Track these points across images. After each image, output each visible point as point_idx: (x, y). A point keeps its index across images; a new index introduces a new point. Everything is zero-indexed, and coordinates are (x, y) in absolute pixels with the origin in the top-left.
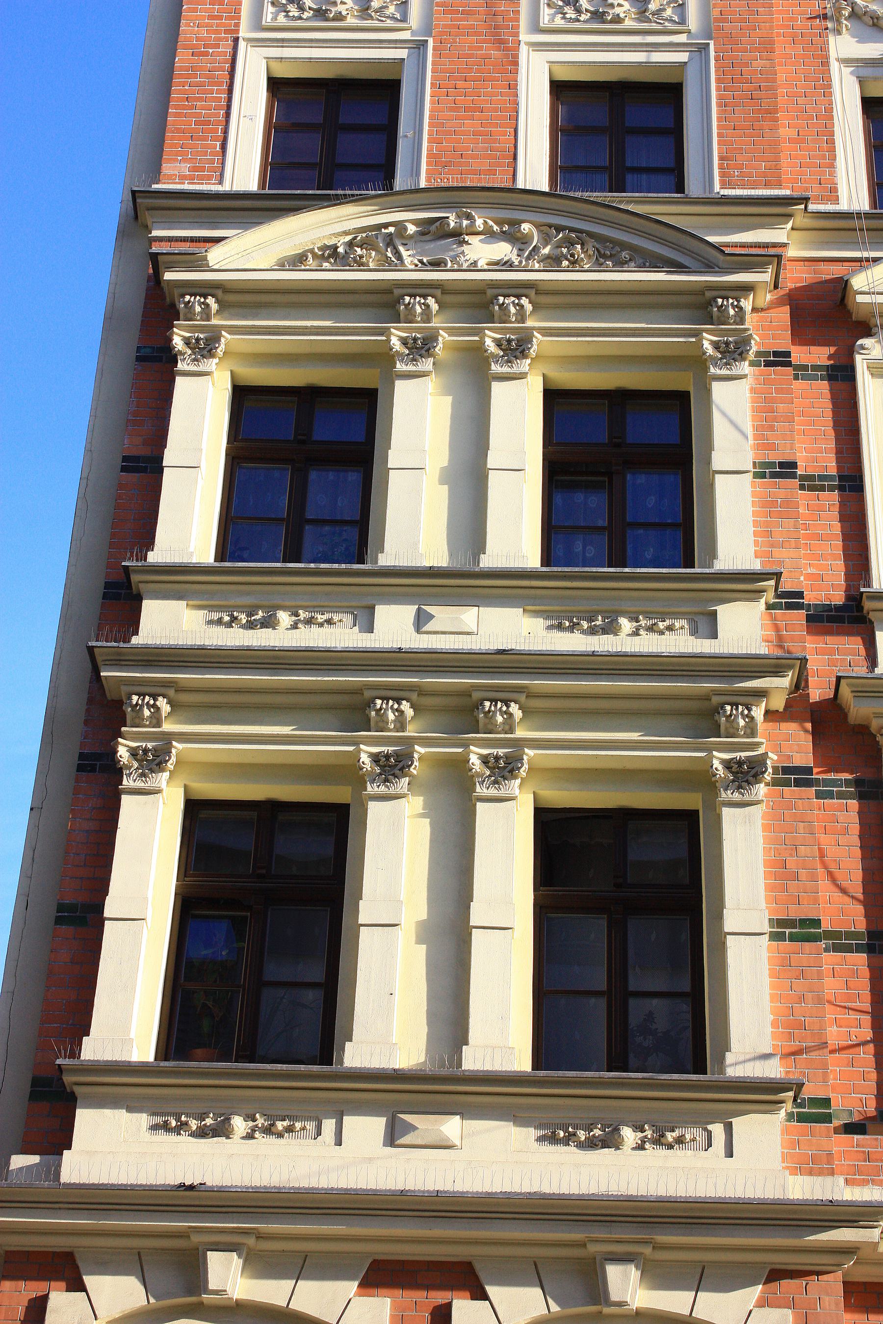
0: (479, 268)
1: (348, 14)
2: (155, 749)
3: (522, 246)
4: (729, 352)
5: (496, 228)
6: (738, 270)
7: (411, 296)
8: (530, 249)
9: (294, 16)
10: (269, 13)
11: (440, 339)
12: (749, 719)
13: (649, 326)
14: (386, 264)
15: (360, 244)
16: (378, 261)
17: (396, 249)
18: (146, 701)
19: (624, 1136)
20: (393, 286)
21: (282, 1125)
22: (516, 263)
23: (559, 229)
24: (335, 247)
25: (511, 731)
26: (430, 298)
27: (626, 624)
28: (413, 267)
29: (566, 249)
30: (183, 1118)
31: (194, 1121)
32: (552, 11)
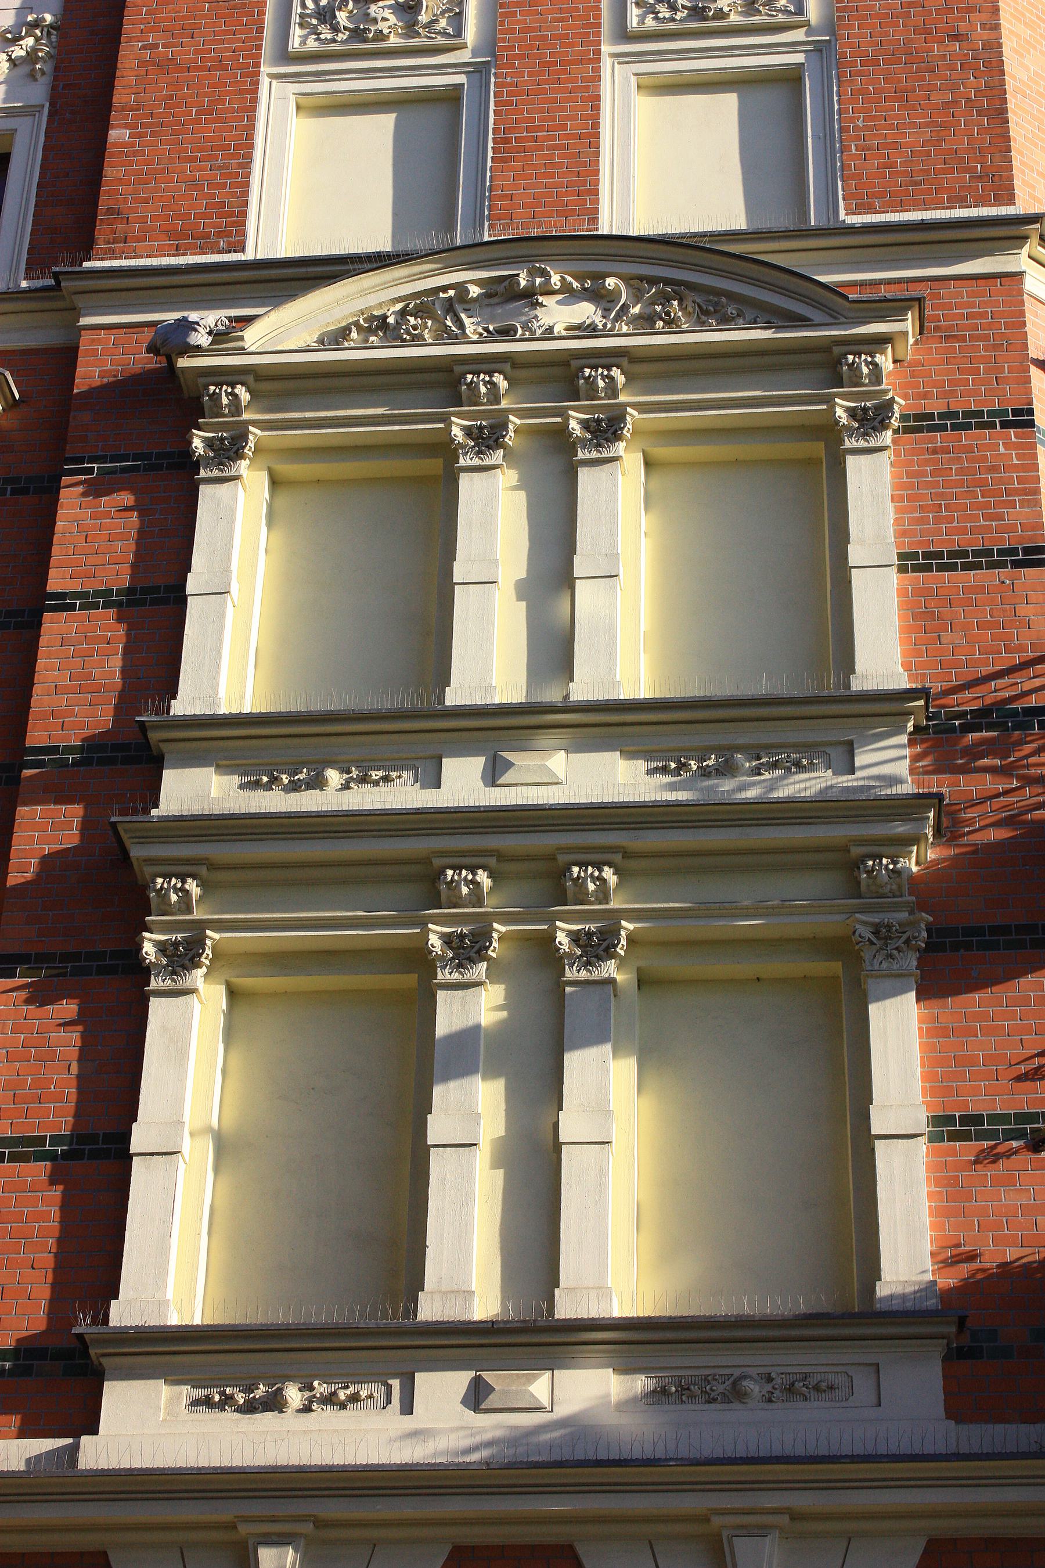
0: (556, 335)
1: (731, 10)
2: (472, 933)
3: (609, 305)
4: (867, 420)
5: (575, 284)
6: (871, 320)
7: (591, 368)
8: (618, 308)
9: (664, 18)
10: (634, 17)
11: (628, 418)
12: (183, 893)
13: (766, 393)
14: (445, 336)
15: (414, 312)
16: (436, 331)
17: (457, 316)
18: (463, 876)
19: (288, 1396)
20: (452, 363)
21: (344, 1394)
22: (601, 327)
23: (652, 281)
24: (385, 317)
25: (606, 900)
26: (614, 369)
27: (334, 777)
28: (475, 337)
29: (660, 307)
30: (228, 1391)
31: (241, 1394)
32: (305, 32)
